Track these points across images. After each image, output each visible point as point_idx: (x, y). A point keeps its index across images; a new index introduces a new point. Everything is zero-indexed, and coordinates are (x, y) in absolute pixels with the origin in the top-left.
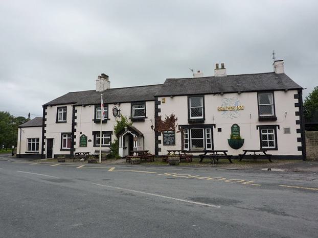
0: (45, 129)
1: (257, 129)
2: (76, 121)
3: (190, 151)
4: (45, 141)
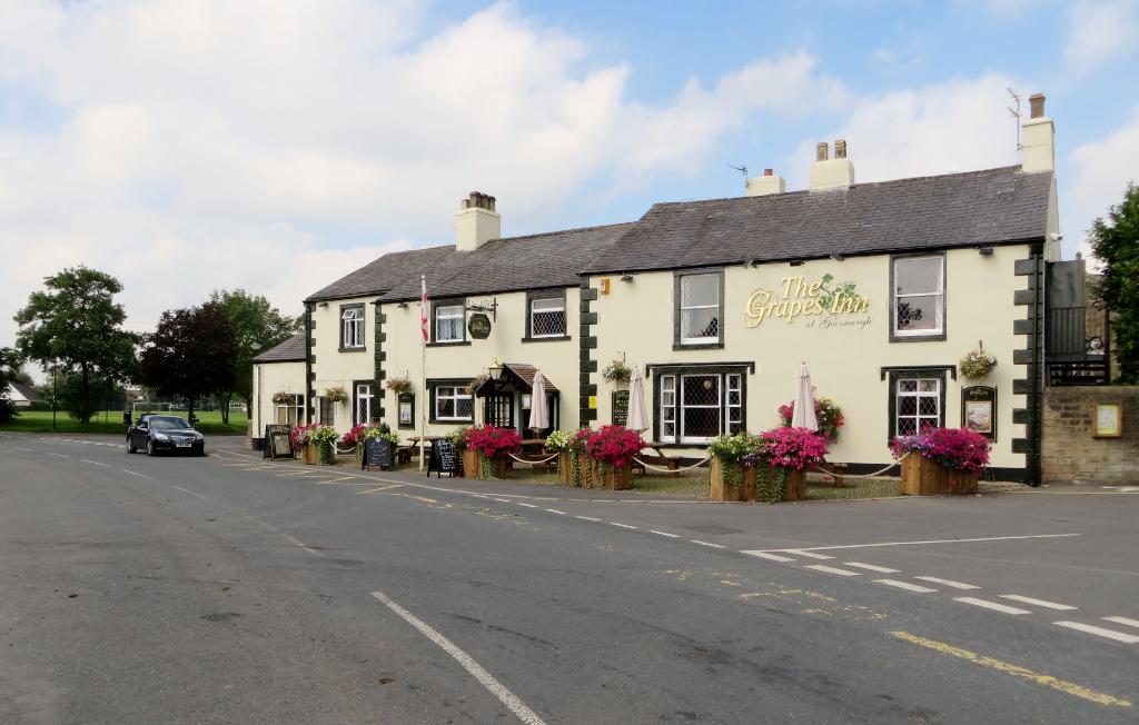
0: (315, 368)
1: (883, 377)
2: (593, 331)
3: (678, 445)
4: (315, 403)
